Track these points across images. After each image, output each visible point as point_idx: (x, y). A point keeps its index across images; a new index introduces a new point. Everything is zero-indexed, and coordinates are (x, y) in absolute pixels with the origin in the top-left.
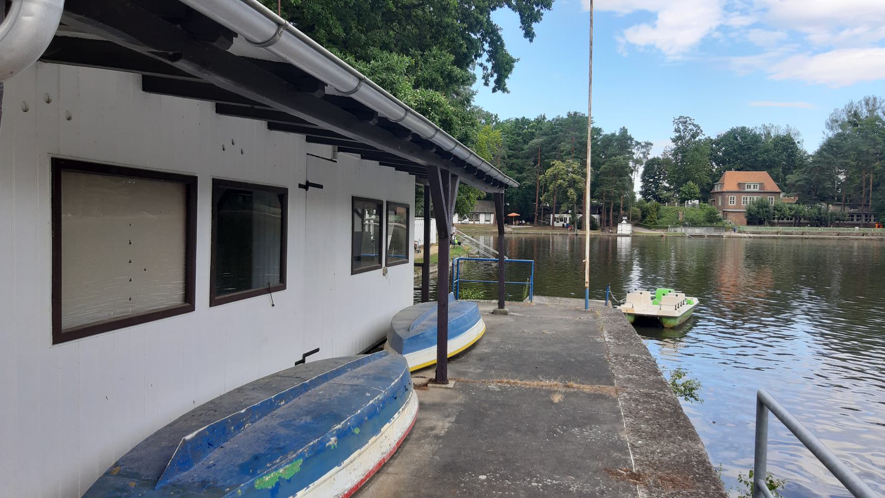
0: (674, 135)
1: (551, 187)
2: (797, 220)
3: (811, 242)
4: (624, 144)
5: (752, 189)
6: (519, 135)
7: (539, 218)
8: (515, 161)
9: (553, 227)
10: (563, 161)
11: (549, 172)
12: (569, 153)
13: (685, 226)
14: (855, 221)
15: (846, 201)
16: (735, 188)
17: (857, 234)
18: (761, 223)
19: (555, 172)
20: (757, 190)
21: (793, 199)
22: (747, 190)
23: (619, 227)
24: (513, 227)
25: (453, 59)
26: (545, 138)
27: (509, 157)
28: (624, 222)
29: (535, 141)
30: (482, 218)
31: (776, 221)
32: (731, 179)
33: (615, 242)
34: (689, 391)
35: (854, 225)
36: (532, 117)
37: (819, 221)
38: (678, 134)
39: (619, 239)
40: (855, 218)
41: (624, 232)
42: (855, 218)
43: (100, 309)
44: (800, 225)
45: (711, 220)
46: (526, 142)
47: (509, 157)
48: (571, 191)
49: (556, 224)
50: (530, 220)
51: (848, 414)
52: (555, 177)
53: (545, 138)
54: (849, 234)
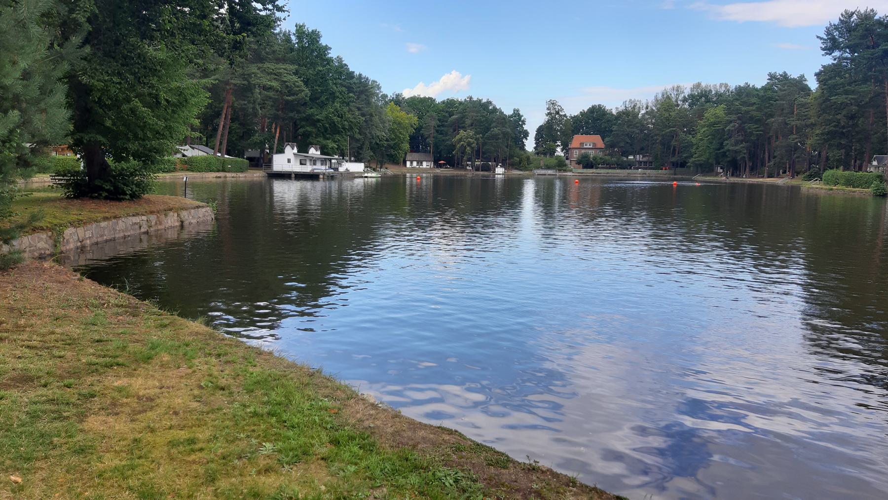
2: (610, 166)
3: (602, 177)
4: (133, 146)
5: (588, 147)
6: (447, 112)
9: (466, 169)
11: (458, 137)
13: (542, 168)
14: (642, 166)
16: (578, 146)
17: (661, 174)
21: (319, 153)
23: (497, 169)
25: (119, 142)
30: (425, 164)
31: (600, 166)
35: (638, 169)
37: (622, 166)
38: (549, 111)
39: (496, 176)
40: (642, 164)
41: (499, 172)
42: (642, 164)
43: (649, 406)
44: (610, 168)
46: (450, 116)
47: (438, 126)
52: (460, 140)
54: (635, 174)
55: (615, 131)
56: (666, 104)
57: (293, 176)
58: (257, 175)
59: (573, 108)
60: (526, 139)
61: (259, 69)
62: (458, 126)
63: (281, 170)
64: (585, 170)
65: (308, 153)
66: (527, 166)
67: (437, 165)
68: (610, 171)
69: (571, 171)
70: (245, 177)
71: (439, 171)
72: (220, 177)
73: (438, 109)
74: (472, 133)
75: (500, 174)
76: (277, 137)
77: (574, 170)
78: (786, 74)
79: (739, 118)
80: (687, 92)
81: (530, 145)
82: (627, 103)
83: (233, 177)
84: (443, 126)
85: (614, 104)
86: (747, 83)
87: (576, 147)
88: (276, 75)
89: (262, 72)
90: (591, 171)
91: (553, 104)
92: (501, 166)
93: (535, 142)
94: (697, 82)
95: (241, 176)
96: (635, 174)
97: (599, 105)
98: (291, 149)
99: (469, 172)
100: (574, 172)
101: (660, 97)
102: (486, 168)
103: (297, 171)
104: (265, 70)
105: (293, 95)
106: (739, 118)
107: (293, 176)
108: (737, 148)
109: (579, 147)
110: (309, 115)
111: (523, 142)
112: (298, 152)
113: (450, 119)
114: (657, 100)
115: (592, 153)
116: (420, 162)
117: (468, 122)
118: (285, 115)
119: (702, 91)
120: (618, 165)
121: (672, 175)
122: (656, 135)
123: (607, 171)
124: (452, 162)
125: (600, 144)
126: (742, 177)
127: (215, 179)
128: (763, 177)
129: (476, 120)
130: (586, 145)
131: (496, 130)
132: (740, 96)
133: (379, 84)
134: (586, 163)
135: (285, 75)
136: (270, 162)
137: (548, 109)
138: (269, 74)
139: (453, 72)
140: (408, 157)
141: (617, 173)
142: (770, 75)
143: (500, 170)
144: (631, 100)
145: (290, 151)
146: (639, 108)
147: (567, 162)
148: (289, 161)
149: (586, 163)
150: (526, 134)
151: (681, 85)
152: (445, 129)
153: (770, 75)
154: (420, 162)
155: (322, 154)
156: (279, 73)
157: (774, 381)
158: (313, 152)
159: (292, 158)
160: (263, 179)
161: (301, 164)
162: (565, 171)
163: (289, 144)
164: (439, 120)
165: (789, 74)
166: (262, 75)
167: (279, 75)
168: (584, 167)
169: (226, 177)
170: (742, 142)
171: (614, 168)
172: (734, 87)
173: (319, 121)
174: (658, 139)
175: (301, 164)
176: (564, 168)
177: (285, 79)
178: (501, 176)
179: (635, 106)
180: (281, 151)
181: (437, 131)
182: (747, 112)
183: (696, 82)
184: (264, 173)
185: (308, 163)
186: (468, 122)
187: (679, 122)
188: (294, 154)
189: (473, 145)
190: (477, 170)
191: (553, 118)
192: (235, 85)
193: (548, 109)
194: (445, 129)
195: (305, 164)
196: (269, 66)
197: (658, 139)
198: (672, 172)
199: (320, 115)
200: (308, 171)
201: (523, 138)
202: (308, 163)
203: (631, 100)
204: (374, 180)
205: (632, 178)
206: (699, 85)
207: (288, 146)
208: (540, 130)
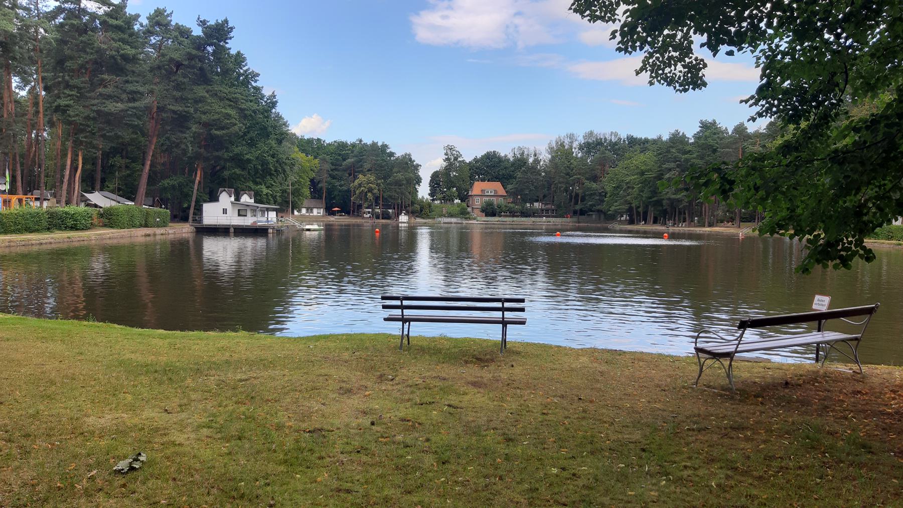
0: (445, 157)
1: (357, 192)
2: (513, 214)
5: (489, 194)
6: (340, 155)
7: (353, 212)
8: (336, 172)
9: (364, 218)
10: (365, 176)
11: (357, 182)
12: (369, 170)
13: (445, 217)
15: (639, 195)
18: (493, 214)
19: (360, 182)
20: (493, 194)
21: (252, 201)
22: (486, 194)
23: (400, 217)
24: (336, 217)
26: (355, 158)
27: (362, 166)
28: (403, 214)
29: (349, 160)
30: (315, 211)
32: (478, 187)
33: (398, 226)
34: (710, 382)
36: (368, 141)
37: (525, 214)
39: (400, 225)
40: (544, 212)
41: (403, 221)
42: (544, 212)
44: (514, 216)
45: (464, 214)
46: (344, 160)
47: (332, 170)
48: (369, 194)
49: (365, 215)
50: (348, 213)
51: (368, 299)
52: (360, 185)
53: (355, 158)
54: (540, 222)
55: (519, 178)
56: (561, 152)
57: (232, 230)
58: (184, 230)
59: (470, 154)
60: (419, 185)
61: (207, 92)
62: (353, 172)
63: (216, 223)
64: (490, 219)
65: (240, 201)
66: (429, 214)
67: (329, 211)
68: (515, 219)
69: (474, 219)
70: (175, 233)
71: (332, 219)
72: (149, 235)
73: (329, 151)
74: (372, 178)
75: (405, 223)
76: (197, 182)
77: (479, 218)
78: (715, 123)
79: (678, 166)
80: (581, 140)
81: (424, 191)
82: (516, 150)
83: (162, 234)
84: (335, 169)
85: (506, 151)
86: (677, 131)
87: (478, 194)
88: (231, 101)
89: (211, 96)
90: (496, 219)
91: (451, 149)
92: (405, 214)
93: (429, 188)
94: (589, 130)
95: (170, 232)
96: (540, 222)
97: (494, 152)
98: (228, 196)
99: (366, 220)
100: (478, 222)
101: (554, 145)
102: (386, 216)
103: (236, 224)
104: (216, 95)
105: (223, 128)
106: (678, 166)
107: (232, 230)
108: (679, 196)
109: (480, 194)
110: (237, 154)
111: (416, 189)
112: (235, 200)
113: (344, 163)
114: (552, 148)
115: (495, 201)
116: (310, 209)
117: (367, 166)
118: (209, 154)
119: (597, 139)
120: (522, 213)
121: (576, 223)
122: (560, 183)
123: (510, 219)
124: (347, 208)
125: (502, 191)
126: (678, 227)
127: (143, 238)
128: (704, 226)
129: (376, 164)
130: (488, 192)
131: (400, 176)
132: (674, 143)
133: (287, 122)
134: (490, 211)
135: (243, 101)
136: (199, 210)
137: (446, 154)
138: (221, 99)
139: (314, 116)
140: (306, 202)
141: (523, 221)
142: (701, 122)
143: (403, 218)
144: (519, 147)
145: (226, 199)
146: (528, 155)
147: (469, 209)
148: (225, 211)
149: (490, 211)
150: (419, 181)
151: (575, 133)
152: (339, 173)
153: (701, 122)
154: (310, 209)
155: (255, 202)
156: (235, 98)
157: (473, 372)
158: (246, 199)
159: (229, 207)
160: (190, 235)
161: (239, 215)
162: (470, 219)
163: (225, 190)
164: (332, 164)
165: (718, 123)
166: (213, 101)
167: (236, 101)
168: (486, 216)
169: (155, 235)
170: (681, 190)
171: (517, 216)
172: (626, 137)
173: (249, 161)
174: (562, 187)
175: (239, 215)
176: (467, 216)
177: (243, 106)
178: (406, 225)
179: (523, 153)
180: (214, 198)
181: (330, 175)
182: (687, 160)
183: (588, 130)
184: (193, 228)
185: (249, 214)
186: (367, 166)
187: (583, 169)
188: (232, 203)
189: (375, 191)
190: (378, 218)
191: (451, 164)
192: (174, 112)
193: (446, 154)
194: (339, 173)
195: (246, 216)
196: (222, 89)
197: (562, 187)
198: (575, 219)
199: (250, 155)
200: (249, 224)
201: (415, 185)
202: (249, 214)
203: (519, 147)
204: (317, 233)
205: (538, 227)
206: (591, 133)
207: (224, 193)
208: (435, 177)
